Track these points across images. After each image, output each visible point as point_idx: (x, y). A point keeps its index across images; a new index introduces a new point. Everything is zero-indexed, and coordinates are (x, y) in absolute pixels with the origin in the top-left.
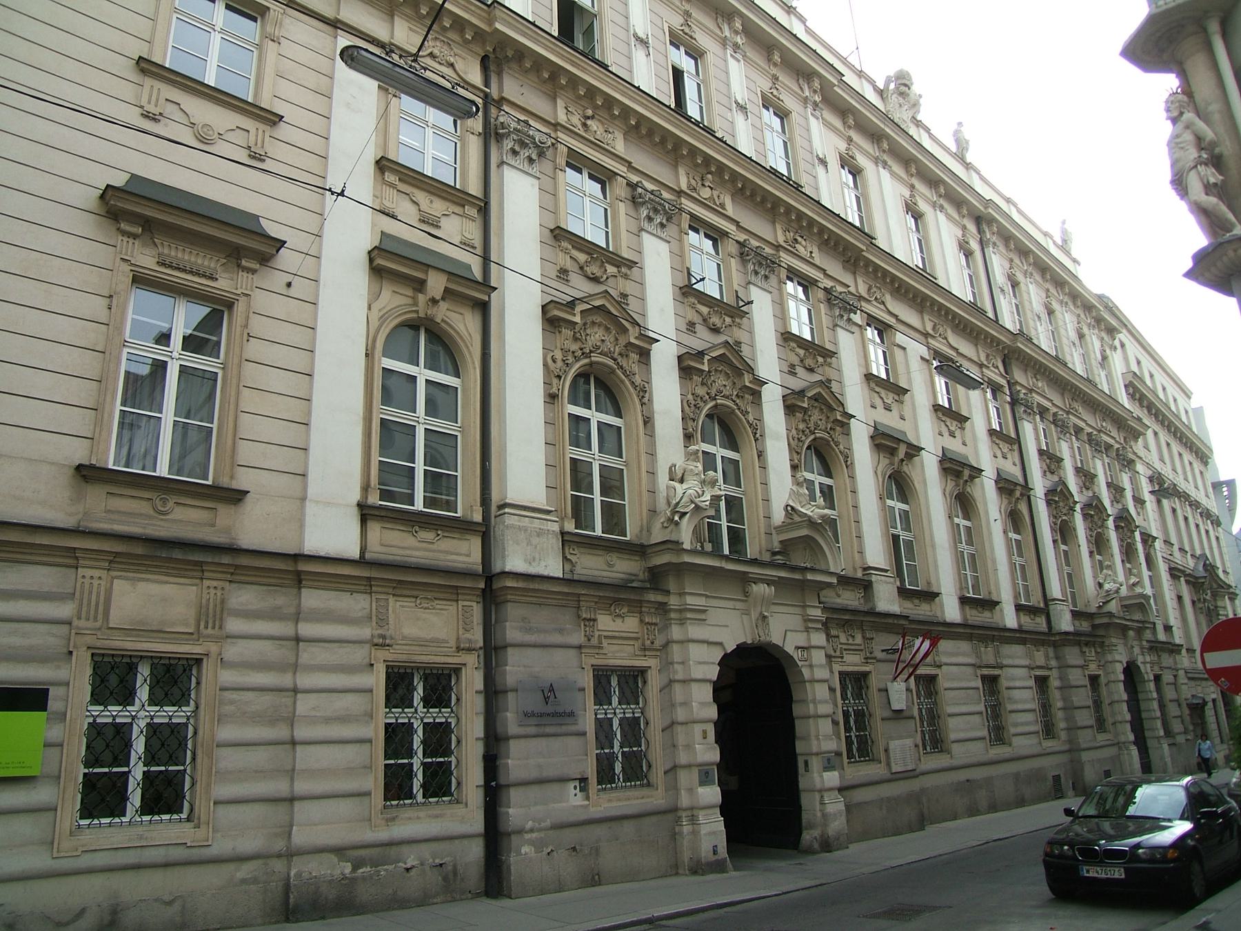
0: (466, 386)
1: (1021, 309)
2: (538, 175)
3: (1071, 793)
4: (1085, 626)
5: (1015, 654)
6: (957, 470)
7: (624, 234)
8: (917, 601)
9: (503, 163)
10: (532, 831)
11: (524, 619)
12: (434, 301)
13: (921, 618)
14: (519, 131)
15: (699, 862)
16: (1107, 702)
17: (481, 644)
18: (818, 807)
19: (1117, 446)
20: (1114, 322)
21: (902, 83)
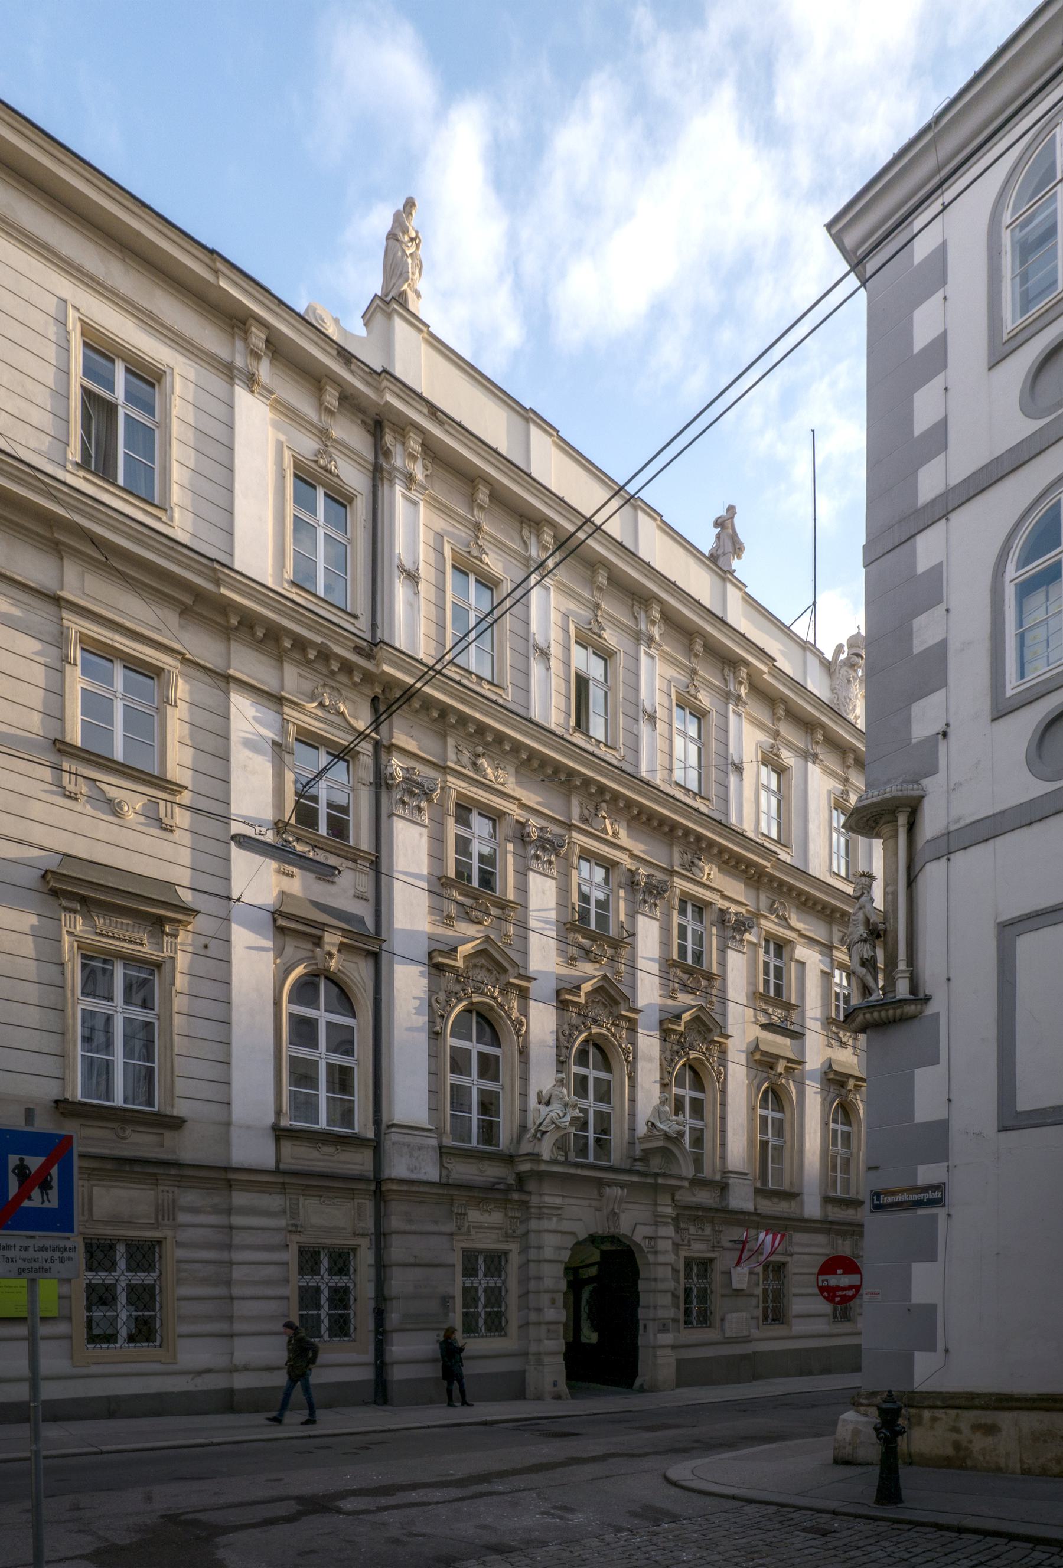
8: (776, 1200)
13: (778, 1214)
17: (373, 1230)
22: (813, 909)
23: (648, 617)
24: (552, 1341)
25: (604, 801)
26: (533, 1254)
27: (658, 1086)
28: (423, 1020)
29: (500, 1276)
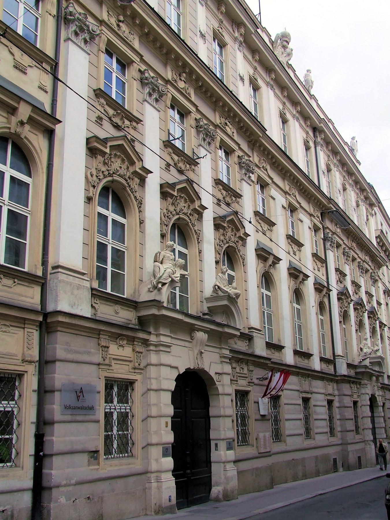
0: (36, 184)
1: (332, 184)
2: (89, 52)
3: (341, 469)
4: (352, 373)
5: (318, 386)
6: (295, 273)
7: (135, 102)
8: (273, 350)
9: (69, 39)
10: (65, 486)
11: (67, 343)
12: (22, 123)
14: (80, 20)
15: (160, 506)
16: (361, 417)
17: (38, 359)
18: (223, 472)
19: (371, 271)
20: (374, 200)
21: (285, 39)
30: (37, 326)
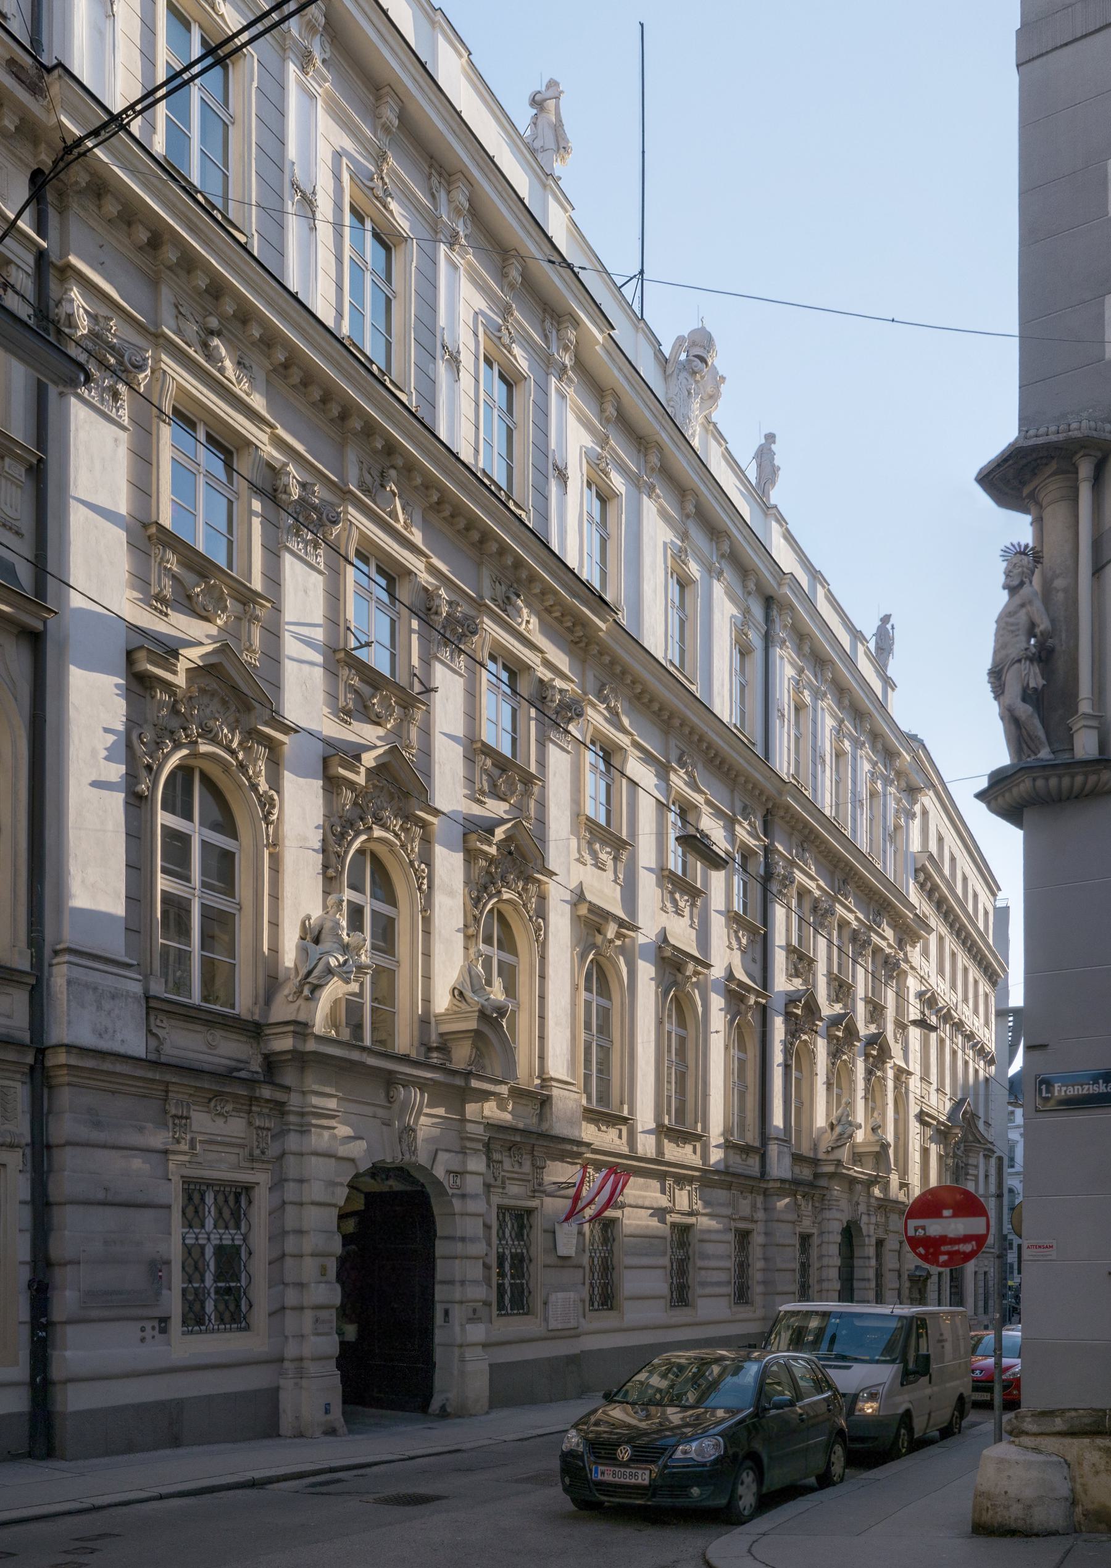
22: (648, 707)
23: (450, 202)
24: (323, 1339)
25: (393, 467)
26: (291, 1191)
27: (461, 935)
28: (116, 771)
29: (238, 1227)
30: (24, 1074)
